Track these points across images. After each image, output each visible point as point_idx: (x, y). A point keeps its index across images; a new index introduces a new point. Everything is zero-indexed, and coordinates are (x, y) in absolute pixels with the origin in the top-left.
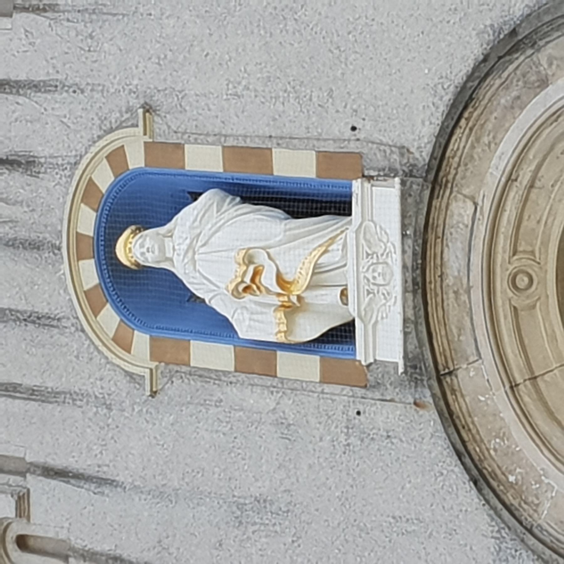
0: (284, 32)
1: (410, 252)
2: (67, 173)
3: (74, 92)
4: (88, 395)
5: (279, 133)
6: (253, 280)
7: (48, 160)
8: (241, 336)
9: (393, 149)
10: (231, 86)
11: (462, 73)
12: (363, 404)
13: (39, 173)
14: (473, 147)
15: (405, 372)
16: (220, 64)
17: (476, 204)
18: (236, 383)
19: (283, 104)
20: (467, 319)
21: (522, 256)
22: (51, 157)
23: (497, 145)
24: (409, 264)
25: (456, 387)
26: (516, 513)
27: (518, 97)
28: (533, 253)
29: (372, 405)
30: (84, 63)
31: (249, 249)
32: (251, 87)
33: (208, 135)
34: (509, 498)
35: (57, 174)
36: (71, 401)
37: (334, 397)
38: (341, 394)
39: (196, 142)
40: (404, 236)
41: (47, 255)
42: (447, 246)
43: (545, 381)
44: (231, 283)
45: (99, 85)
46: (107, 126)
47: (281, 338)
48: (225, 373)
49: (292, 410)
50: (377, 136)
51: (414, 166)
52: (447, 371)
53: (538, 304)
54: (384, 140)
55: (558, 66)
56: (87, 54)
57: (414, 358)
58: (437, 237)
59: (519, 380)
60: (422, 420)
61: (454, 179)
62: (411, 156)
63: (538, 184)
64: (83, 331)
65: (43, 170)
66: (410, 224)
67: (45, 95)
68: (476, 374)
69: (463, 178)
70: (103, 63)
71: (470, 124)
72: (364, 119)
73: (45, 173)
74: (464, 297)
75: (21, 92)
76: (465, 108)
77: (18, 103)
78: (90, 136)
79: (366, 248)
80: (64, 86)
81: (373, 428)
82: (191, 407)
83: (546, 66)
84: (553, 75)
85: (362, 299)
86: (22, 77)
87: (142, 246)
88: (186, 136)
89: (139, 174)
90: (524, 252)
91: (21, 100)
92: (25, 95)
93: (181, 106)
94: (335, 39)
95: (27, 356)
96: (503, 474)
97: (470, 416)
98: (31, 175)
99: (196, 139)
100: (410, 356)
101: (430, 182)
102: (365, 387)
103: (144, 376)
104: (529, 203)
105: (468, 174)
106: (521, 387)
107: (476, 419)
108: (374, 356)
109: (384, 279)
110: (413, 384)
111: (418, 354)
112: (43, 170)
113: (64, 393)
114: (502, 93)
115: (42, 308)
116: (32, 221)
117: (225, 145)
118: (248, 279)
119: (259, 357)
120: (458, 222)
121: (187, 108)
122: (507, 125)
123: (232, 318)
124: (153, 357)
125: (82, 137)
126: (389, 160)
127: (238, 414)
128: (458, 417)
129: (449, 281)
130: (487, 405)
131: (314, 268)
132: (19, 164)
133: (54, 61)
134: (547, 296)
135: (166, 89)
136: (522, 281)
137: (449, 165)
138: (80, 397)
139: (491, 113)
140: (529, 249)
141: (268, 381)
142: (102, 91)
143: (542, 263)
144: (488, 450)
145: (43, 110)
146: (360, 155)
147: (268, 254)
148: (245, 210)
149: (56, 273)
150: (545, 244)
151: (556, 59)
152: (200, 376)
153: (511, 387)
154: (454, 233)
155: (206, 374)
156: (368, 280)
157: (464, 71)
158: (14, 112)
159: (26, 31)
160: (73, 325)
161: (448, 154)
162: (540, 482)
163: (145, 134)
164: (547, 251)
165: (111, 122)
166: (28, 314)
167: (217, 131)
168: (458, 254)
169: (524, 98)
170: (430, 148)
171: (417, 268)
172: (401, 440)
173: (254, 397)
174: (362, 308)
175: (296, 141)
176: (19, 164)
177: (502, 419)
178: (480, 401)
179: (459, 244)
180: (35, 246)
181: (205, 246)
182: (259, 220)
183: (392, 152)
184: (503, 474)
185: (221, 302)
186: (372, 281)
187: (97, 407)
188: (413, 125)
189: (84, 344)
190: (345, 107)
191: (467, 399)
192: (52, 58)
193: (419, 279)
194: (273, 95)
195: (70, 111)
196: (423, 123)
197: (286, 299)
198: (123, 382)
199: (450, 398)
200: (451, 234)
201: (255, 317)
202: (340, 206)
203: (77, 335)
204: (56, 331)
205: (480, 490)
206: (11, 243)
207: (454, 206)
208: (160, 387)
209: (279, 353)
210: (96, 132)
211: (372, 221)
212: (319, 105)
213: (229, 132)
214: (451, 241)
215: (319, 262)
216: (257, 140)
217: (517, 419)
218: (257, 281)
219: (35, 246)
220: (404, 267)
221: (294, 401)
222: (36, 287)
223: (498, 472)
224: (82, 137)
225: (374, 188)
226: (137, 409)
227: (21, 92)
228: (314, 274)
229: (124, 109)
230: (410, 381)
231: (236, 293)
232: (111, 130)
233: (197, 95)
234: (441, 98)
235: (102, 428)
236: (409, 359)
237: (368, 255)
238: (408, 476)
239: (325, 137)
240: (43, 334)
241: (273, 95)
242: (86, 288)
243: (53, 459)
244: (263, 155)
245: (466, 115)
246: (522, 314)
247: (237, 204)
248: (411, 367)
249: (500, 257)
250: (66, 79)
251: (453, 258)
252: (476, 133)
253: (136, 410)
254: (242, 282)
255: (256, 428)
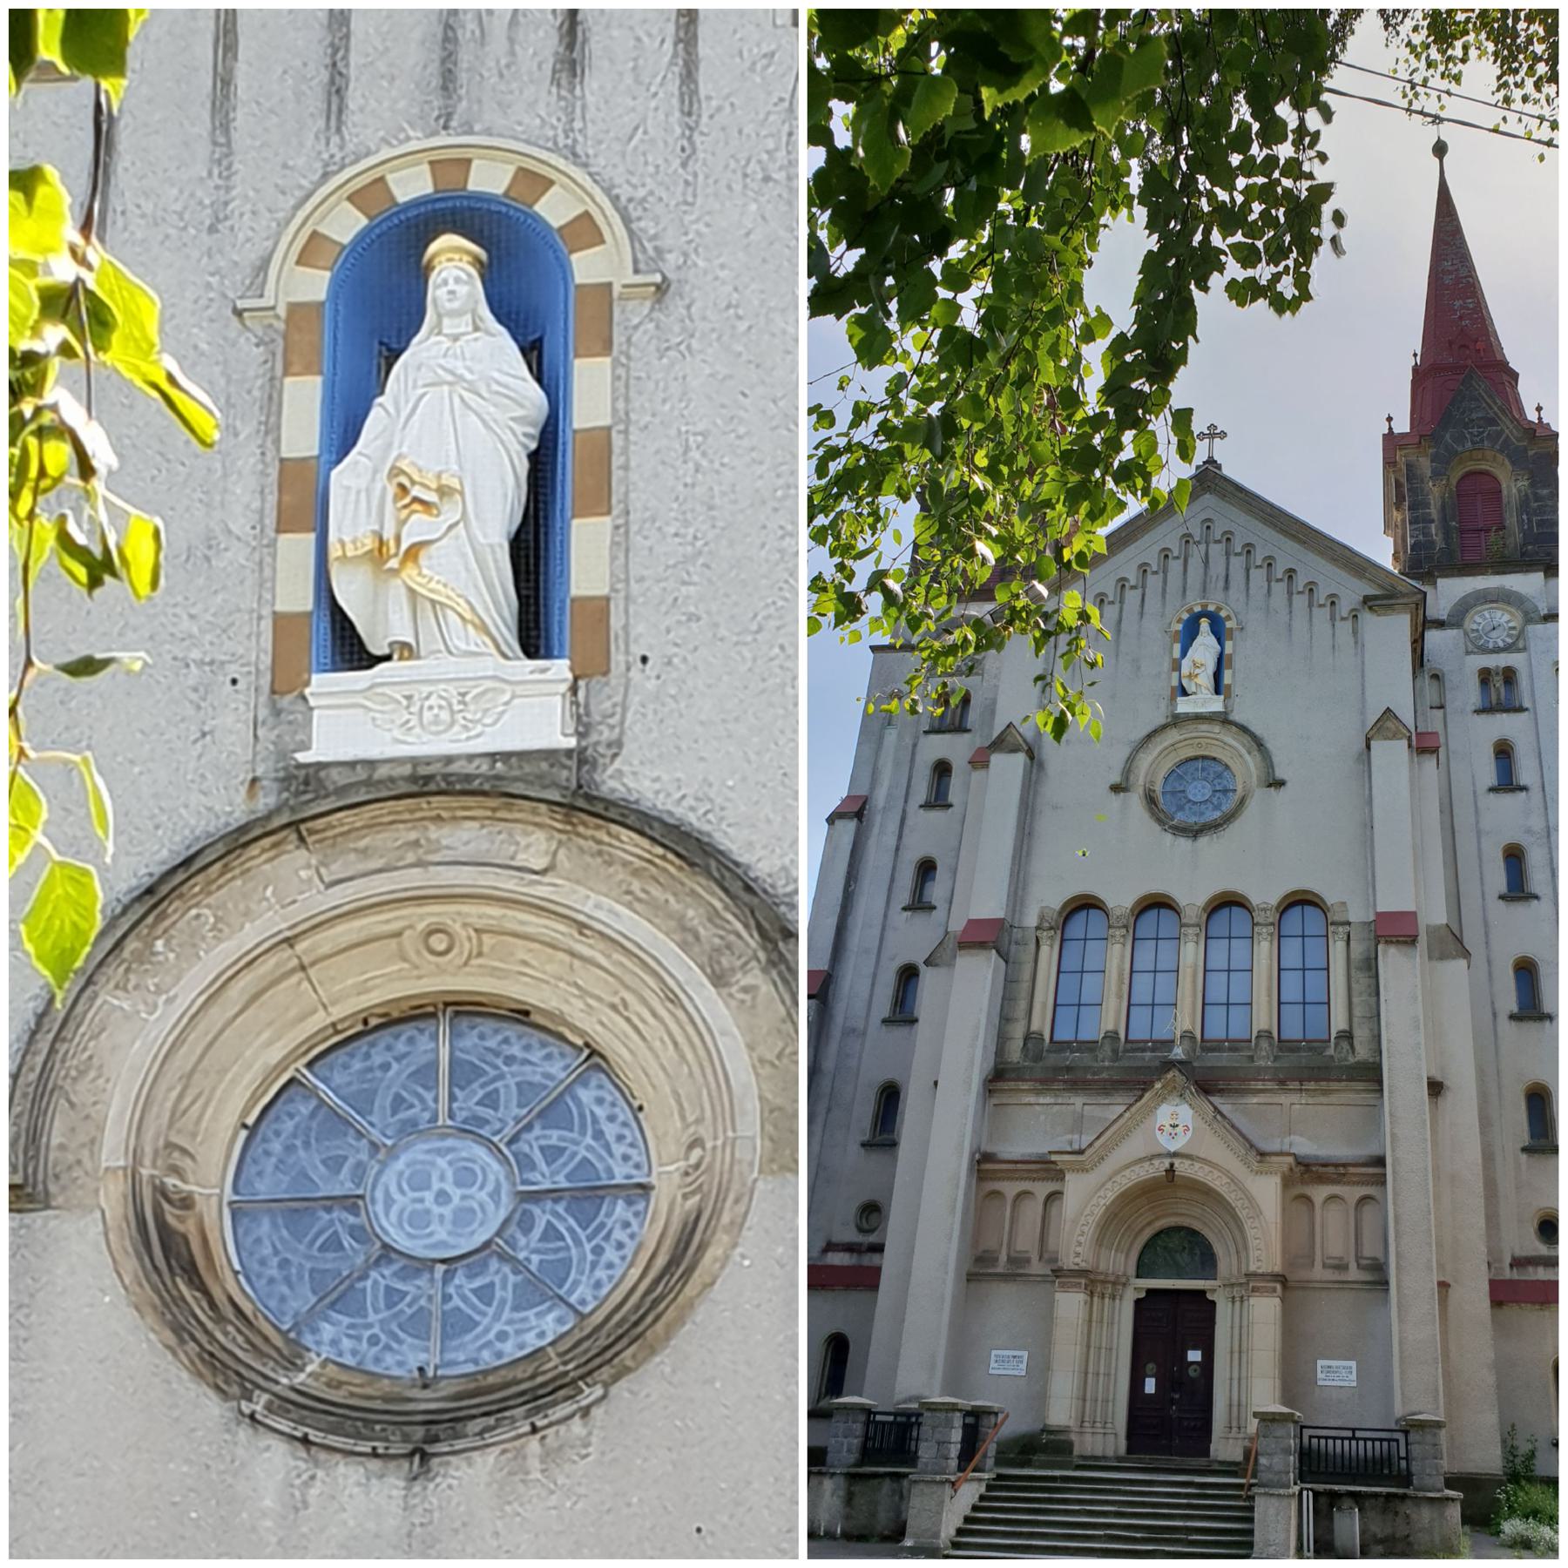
0: (780, 533)
1: (470, 769)
2: (561, 141)
3: (683, 150)
4: (228, 189)
5: (634, 528)
6: (416, 500)
7: (579, 104)
8: (334, 473)
9: (617, 730)
10: (700, 438)
11: (727, 842)
12: (248, 689)
13: (559, 85)
14: (625, 864)
15: (300, 766)
16: (732, 418)
17: (543, 872)
18: (263, 462)
19: (676, 535)
20: (378, 863)
21: (475, 941)
22: (584, 107)
23: (629, 906)
24: (455, 768)
25: (282, 848)
26: (111, 958)
27: (697, 937)
28: (480, 954)
29: (247, 704)
30: (727, 166)
31: (462, 493)
32: (700, 476)
33: (627, 400)
34: (132, 945)
35: (559, 120)
36: (217, 156)
37: (254, 639)
38: (258, 649)
39: (616, 378)
40: (493, 757)
41: (436, 103)
42: (483, 827)
43: (299, 983)
44: (413, 464)
45: (695, 196)
46: (635, 213)
47: (334, 551)
48: (277, 442)
49: (231, 563)
50: (635, 700)
51: (594, 765)
52: (305, 833)
53: (406, 965)
54: (629, 715)
55: (743, 1002)
56: (739, 174)
57: (320, 781)
58: (494, 810)
59: (301, 947)
60: (232, 792)
61: (579, 835)
62: (607, 760)
63: (577, 963)
64: (326, 176)
65: (564, 93)
66: (511, 768)
67: (676, 93)
68: (302, 881)
69: (581, 849)
70: (728, 204)
71: (657, 861)
72: (658, 677)
73: (560, 98)
74: (410, 857)
75: (681, 46)
76: (678, 855)
77: (663, 41)
78: (617, 181)
79: (475, 691)
80: (691, 129)
81: (214, 708)
82: (222, 382)
83: (743, 983)
84: (731, 995)
85: (397, 688)
86: (703, 49)
87: (457, 280)
88: (623, 360)
89: (565, 270)
90: (480, 943)
91: (668, 45)
92: (675, 55)
93: (668, 349)
94: (773, 623)
95: (280, 70)
96: (165, 931)
97: (242, 873)
98: (554, 71)
99: (619, 378)
100: (322, 774)
101: (570, 793)
102: (273, 692)
103: (261, 296)
104: (550, 951)
105: (588, 859)
106: (290, 951)
107: (239, 882)
108: (319, 707)
109: (431, 723)
110: (281, 774)
111: (325, 788)
112: (564, 93)
113: (229, 144)
114: (701, 911)
115: (354, 99)
116: (486, 74)
117: (614, 434)
118: (416, 491)
119: (1177, 666)
120: (518, 844)
121: (665, 360)
122: (657, 921)
123: (360, 453)
124: (294, 308)
125: (615, 166)
126: (600, 723)
127: (218, 465)
128: (239, 856)
129: (434, 832)
130: (260, 901)
131: (441, 604)
132: (571, 47)
133: (728, 109)
134: (419, 977)
135: (692, 320)
136: (439, 942)
137: (598, 827)
138: (225, 174)
139: (675, 895)
140: (485, 949)
141: (270, 521)
142: (686, 203)
143: (467, 969)
144: (197, 905)
145: (653, 89)
146: (606, 673)
147: (457, 523)
148: (519, 470)
149: (409, 123)
150: (494, 972)
151: (754, 998)
152: (270, 398)
153: (286, 940)
154: (501, 837)
155: (274, 408)
156: (427, 698)
157: (734, 848)
158: (649, 35)
159: (773, 54)
160: (332, 156)
161: (615, 828)
162: (159, 990)
163: (625, 286)
164: (482, 975)
165: (639, 219)
166: (344, 71)
167: (633, 416)
168: (472, 845)
169: (696, 949)
170: (621, 792)
171: (448, 783)
172: (200, 757)
173: (1167, 665)
174: (387, 690)
175: (622, 559)
176: (571, 47)
177: (242, 927)
178: (265, 888)
179: (485, 846)
180: (1204, 590)
181: (1205, 648)
182: (506, 496)
183: (612, 727)
184: (165, 931)
185: (380, 428)
186: (427, 704)
187: (212, 204)
188: (652, 762)
189: (305, 177)
190: (676, 645)
191: (267, 867)
192: (732, 105)
193: (432, 787)
194: (689, 516)
195: (653, 141)
196: (657, 780)
197: (393, 551)
198: (252, 255)
199: (267, 842)
200: (500, 833)
201: (363, 496)
202: (1217, 691)
203: (318, 165)
204: (321, 123)
205: (139, 899)
206: (450, 34)
207: (540, 835)
208: (248, 323)
209: (312, 536)
210: (624, 192)
211: (513, 697)
212: (676, 599)
213: (632, 438)
214: (490, 833)
215: (450, 613)
216: (623, 489)
217: (244, 950)
218: (416, 506)
219: (1204, 590)
220: (449, 759)
221: (243, 567)
222: (385, 84)
223: (167, 923)
224: (615, 166)
225: (559, 698)
226: (214, 280)
227: (681, 46)
228: (433, 602)
229: (658, 243)
230: (285, 769)
231: (395, 471)
232: (627, 221)
233: (684, 378)
234: (692, 809)
235: (181, 216)
236: (317, 772)
237: (463, 695)
238: (149, 771)
239: (631, 611)
240: (315, 100)
241: (689, 516)
242: (390, 178)
243: (126, 126)
244: (599, 502)
245: (670, 856)
246: (393, 943)
247: (525, 446)
248: (307, 776)
249: (471, 910)
250: (702, 133)
251: (465, 836)
252: (645, 869)
253: (211, 279)
254: (413, 483)
255: (201, 501)
